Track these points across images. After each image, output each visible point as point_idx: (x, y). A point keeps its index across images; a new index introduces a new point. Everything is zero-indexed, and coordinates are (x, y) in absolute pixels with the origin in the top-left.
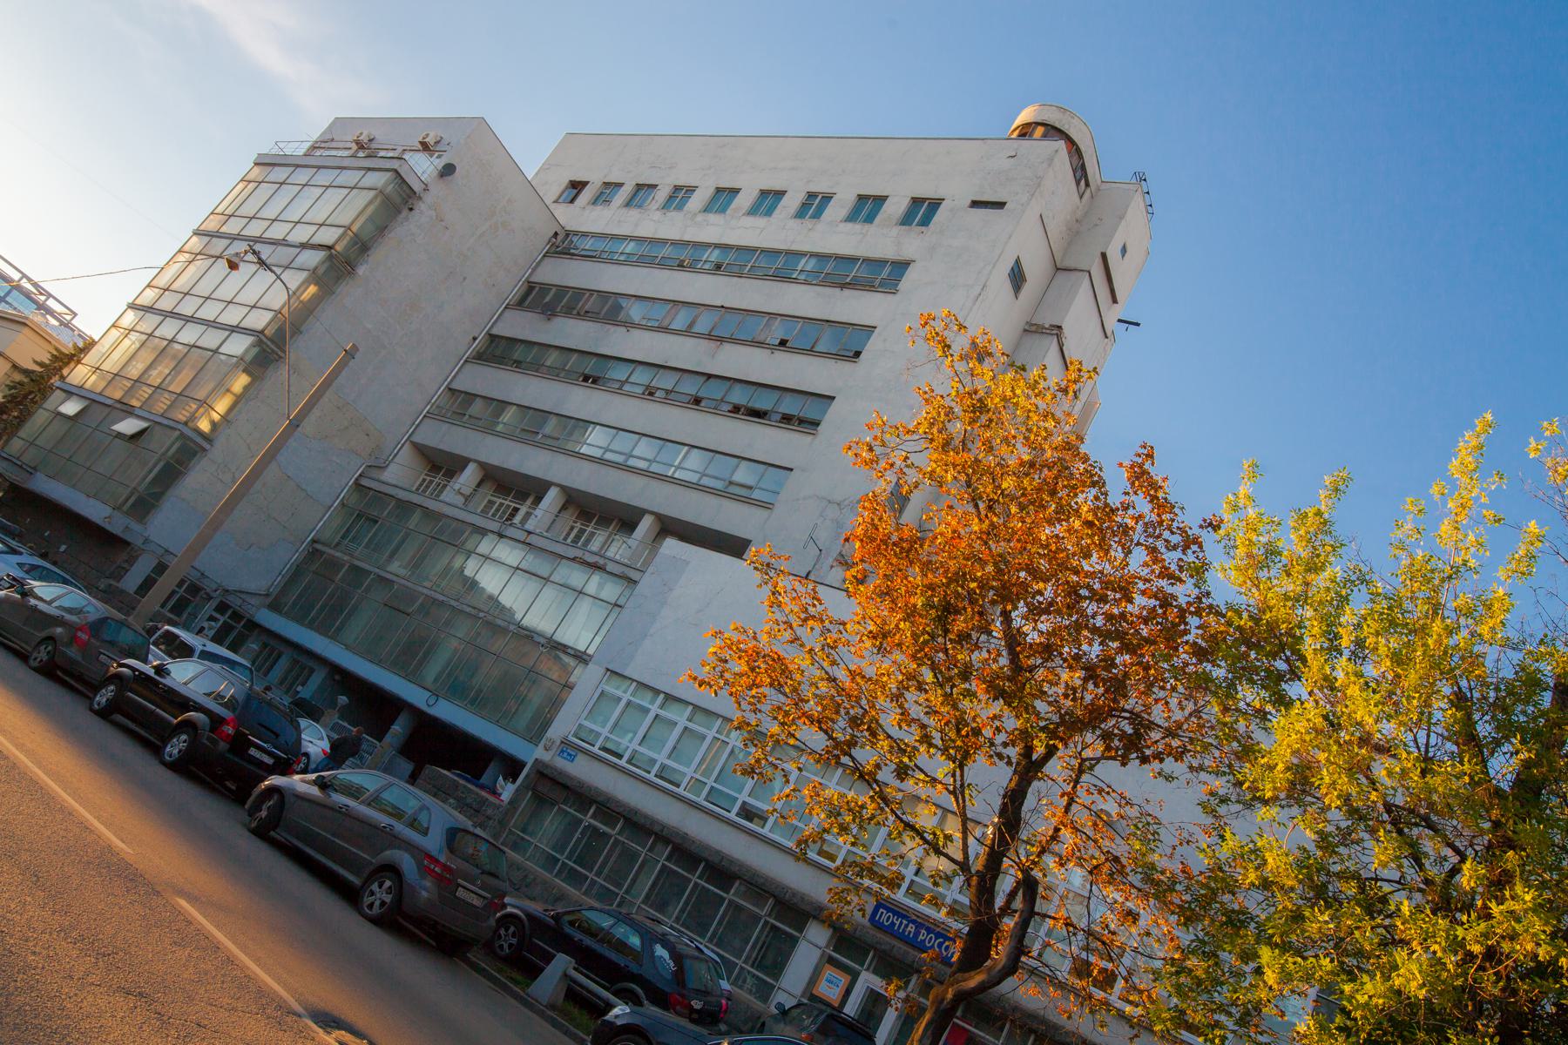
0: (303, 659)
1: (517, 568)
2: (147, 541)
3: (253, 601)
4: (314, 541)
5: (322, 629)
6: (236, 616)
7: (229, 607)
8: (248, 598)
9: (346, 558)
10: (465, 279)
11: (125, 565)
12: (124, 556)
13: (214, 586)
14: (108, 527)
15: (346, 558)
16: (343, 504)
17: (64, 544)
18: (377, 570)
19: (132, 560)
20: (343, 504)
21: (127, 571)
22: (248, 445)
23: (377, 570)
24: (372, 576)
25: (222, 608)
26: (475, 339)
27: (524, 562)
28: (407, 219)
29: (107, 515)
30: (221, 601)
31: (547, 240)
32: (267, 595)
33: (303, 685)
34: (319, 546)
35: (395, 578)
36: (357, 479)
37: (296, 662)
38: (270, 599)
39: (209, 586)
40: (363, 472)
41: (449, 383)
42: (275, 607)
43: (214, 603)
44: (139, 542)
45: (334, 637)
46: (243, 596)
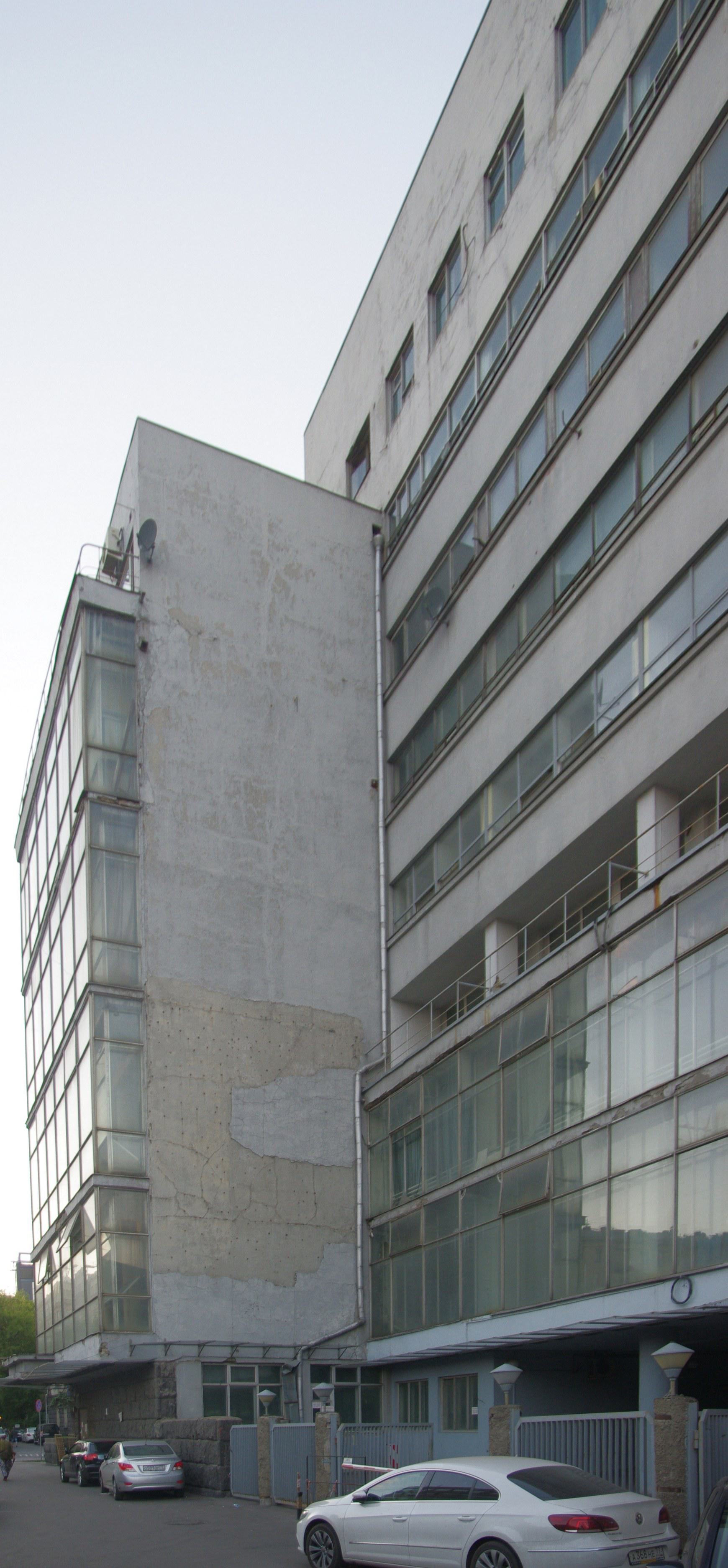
0: (454, 1371)
1: (680, 1151)
2: (167, 1345)
3: (350, 1341)
4: (367, 1221)
5: (448, 1317)
6: (346, 1373)
7: (328, 1368)
8: (342, 1342)
9: (414, 1205)
10: (296, 701)
11: (166, 1392)
12: (156, 1383)
13: (290, 1353)
14: (112, 1359)
15: (414, 1205)
16: (368, 1148)
17: (119, 1412)
18: (460, 1185)
19: (170, 1381)
20: (370, 1148)
21: (175, 1397)
22: (192, 1149)
23: (460, 1185)
24: (461, 1198)
25: (320, 1373)
26: (375, 785)
27: (682, 1132)
28: (149, 668)
29: (98, 1346)
30: (312, 1366)
31: (368, 549)
32: (361, 1325)
33: (476, 1405)
34: (374, 1223)
35: (491, 1171)
36: (362, 1103)
37: (448, 1380)
38: (369, 1329)
39: (284, 1356)
40: (362, 1088)
41: (387, 876)
42: (381, 1332)
43: (305, 1373)
44: (158, 1354)
45: (469, 1314)
46: (333, 1343)
